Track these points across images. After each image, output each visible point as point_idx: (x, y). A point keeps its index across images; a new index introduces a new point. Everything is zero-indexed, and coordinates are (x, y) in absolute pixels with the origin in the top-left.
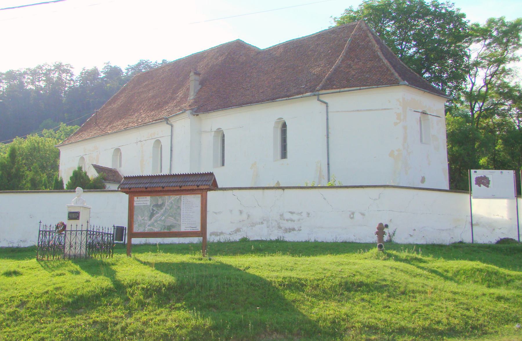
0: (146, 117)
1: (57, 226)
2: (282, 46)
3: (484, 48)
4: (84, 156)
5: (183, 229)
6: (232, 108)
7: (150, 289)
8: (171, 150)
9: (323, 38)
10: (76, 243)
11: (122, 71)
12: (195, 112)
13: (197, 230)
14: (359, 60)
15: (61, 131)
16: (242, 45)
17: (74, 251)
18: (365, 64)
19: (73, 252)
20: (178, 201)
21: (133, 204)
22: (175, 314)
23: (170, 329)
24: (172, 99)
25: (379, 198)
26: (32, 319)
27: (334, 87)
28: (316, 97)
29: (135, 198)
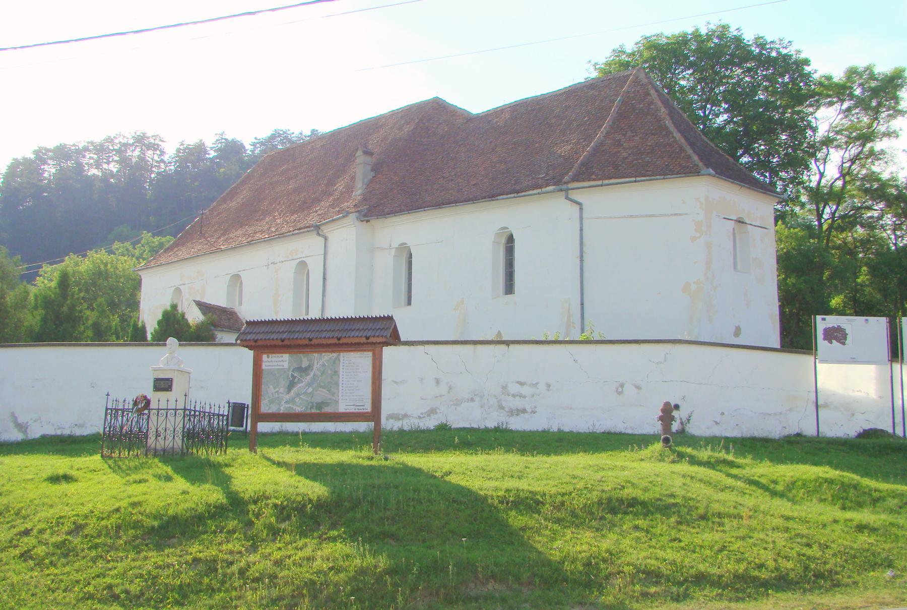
1: (136, 401)
2: (509, 109)
3: (840, 116)
5: (342, 408)
7: (287, 506)
8: (324, 279)
10: (166, 430)
11: (244, 147)
12: (364, 216)
17: (162, 442)
19: (160, 444)
20: (334, 362)
21: (261, 365)
22: (328, 549)
24: (327, 194)
25: (665, 360)
26: (93, 553)
27: (593, 177)
28: (563, 193)
29: (265, 357)
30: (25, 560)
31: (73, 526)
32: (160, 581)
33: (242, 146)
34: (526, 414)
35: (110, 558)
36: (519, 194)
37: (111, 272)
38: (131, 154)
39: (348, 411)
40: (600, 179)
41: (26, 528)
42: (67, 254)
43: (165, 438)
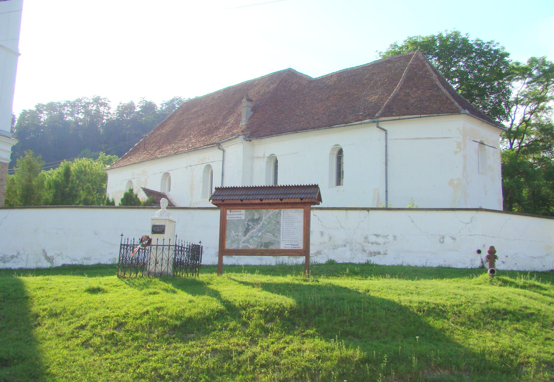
0: (196, 142)
1: (142, 240)
2: (336, 75)
3: (525, 86)
4: (133, 180)
5: (282, 247)
6: (286, 134)
7: (270, 311)
8: (223, 175)
9: (378, 67)
10: (162, 259)
11: (156, 106)
12: (249, 137)
13: (298, 248)
14: (418, 89)
15: (100, 160)
16: (294, 73)
17: (160, 268)
18: (424, 93)
19: (159, 269)
20: (277, 215)
21: (225, 218)
22: (309, 344)
23: (310, 360)
24: (223, 125)
25: (471, 221)
26: (136, 344)
27: (394, 114)
28: (375, 124)
29: (228, 212)
30: (87, 348)
31: (116, 324)
32: (192, 365)
33: (155, 105)
34: (380, 255)
35: (149, 348)
36: (347, 124)
37: (88, 171)
38: (91, 108)
39: (287, 248)
40: (398, 116)
41: (82, 324)
42: (62, 160)
43: (162, 265)
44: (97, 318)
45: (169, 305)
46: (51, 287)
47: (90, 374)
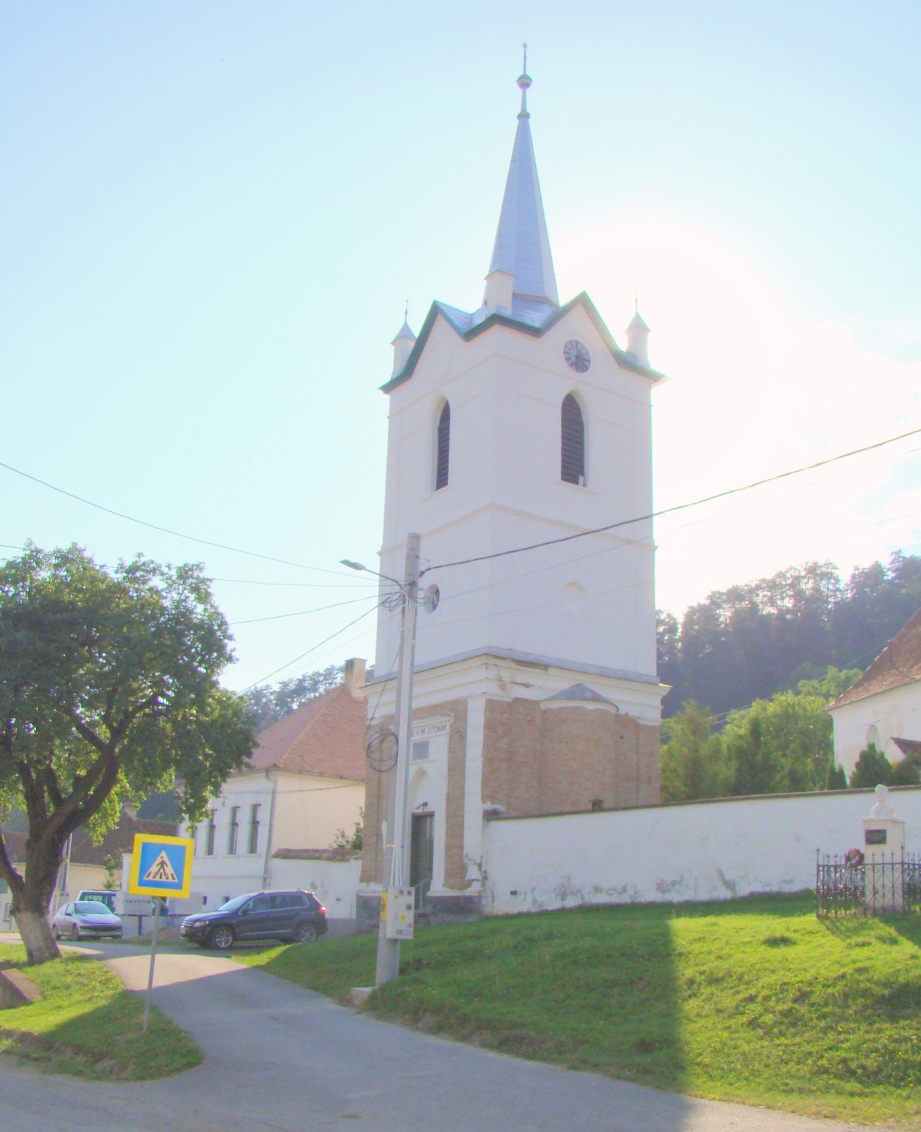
4: (877, 725)
19: (879, 902)
26: (823, 1024)
30: (754, 1029)
31: (798, 994)
32: (898, 1056)
43: (884, 895)
44: (772, 985)
45: (878, 963)
46: (715, 937)
47: (753, 1066)
